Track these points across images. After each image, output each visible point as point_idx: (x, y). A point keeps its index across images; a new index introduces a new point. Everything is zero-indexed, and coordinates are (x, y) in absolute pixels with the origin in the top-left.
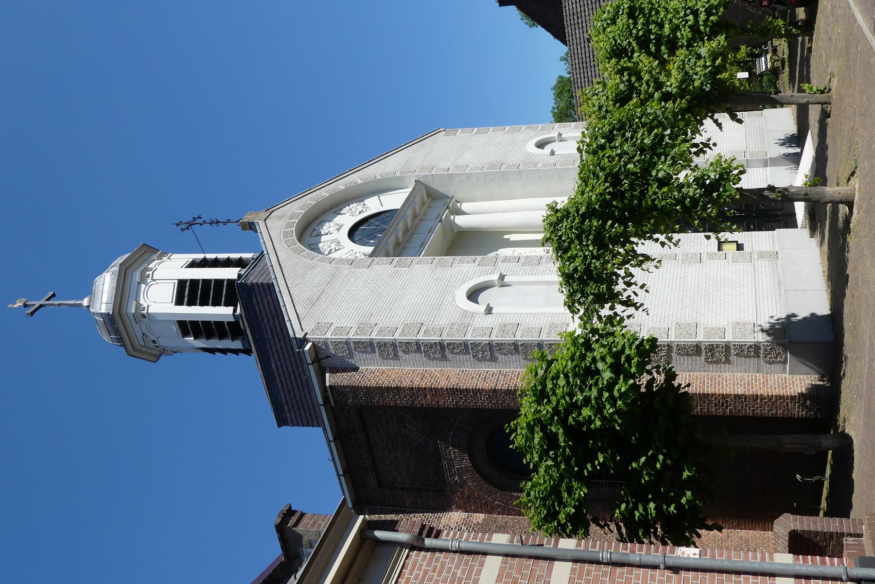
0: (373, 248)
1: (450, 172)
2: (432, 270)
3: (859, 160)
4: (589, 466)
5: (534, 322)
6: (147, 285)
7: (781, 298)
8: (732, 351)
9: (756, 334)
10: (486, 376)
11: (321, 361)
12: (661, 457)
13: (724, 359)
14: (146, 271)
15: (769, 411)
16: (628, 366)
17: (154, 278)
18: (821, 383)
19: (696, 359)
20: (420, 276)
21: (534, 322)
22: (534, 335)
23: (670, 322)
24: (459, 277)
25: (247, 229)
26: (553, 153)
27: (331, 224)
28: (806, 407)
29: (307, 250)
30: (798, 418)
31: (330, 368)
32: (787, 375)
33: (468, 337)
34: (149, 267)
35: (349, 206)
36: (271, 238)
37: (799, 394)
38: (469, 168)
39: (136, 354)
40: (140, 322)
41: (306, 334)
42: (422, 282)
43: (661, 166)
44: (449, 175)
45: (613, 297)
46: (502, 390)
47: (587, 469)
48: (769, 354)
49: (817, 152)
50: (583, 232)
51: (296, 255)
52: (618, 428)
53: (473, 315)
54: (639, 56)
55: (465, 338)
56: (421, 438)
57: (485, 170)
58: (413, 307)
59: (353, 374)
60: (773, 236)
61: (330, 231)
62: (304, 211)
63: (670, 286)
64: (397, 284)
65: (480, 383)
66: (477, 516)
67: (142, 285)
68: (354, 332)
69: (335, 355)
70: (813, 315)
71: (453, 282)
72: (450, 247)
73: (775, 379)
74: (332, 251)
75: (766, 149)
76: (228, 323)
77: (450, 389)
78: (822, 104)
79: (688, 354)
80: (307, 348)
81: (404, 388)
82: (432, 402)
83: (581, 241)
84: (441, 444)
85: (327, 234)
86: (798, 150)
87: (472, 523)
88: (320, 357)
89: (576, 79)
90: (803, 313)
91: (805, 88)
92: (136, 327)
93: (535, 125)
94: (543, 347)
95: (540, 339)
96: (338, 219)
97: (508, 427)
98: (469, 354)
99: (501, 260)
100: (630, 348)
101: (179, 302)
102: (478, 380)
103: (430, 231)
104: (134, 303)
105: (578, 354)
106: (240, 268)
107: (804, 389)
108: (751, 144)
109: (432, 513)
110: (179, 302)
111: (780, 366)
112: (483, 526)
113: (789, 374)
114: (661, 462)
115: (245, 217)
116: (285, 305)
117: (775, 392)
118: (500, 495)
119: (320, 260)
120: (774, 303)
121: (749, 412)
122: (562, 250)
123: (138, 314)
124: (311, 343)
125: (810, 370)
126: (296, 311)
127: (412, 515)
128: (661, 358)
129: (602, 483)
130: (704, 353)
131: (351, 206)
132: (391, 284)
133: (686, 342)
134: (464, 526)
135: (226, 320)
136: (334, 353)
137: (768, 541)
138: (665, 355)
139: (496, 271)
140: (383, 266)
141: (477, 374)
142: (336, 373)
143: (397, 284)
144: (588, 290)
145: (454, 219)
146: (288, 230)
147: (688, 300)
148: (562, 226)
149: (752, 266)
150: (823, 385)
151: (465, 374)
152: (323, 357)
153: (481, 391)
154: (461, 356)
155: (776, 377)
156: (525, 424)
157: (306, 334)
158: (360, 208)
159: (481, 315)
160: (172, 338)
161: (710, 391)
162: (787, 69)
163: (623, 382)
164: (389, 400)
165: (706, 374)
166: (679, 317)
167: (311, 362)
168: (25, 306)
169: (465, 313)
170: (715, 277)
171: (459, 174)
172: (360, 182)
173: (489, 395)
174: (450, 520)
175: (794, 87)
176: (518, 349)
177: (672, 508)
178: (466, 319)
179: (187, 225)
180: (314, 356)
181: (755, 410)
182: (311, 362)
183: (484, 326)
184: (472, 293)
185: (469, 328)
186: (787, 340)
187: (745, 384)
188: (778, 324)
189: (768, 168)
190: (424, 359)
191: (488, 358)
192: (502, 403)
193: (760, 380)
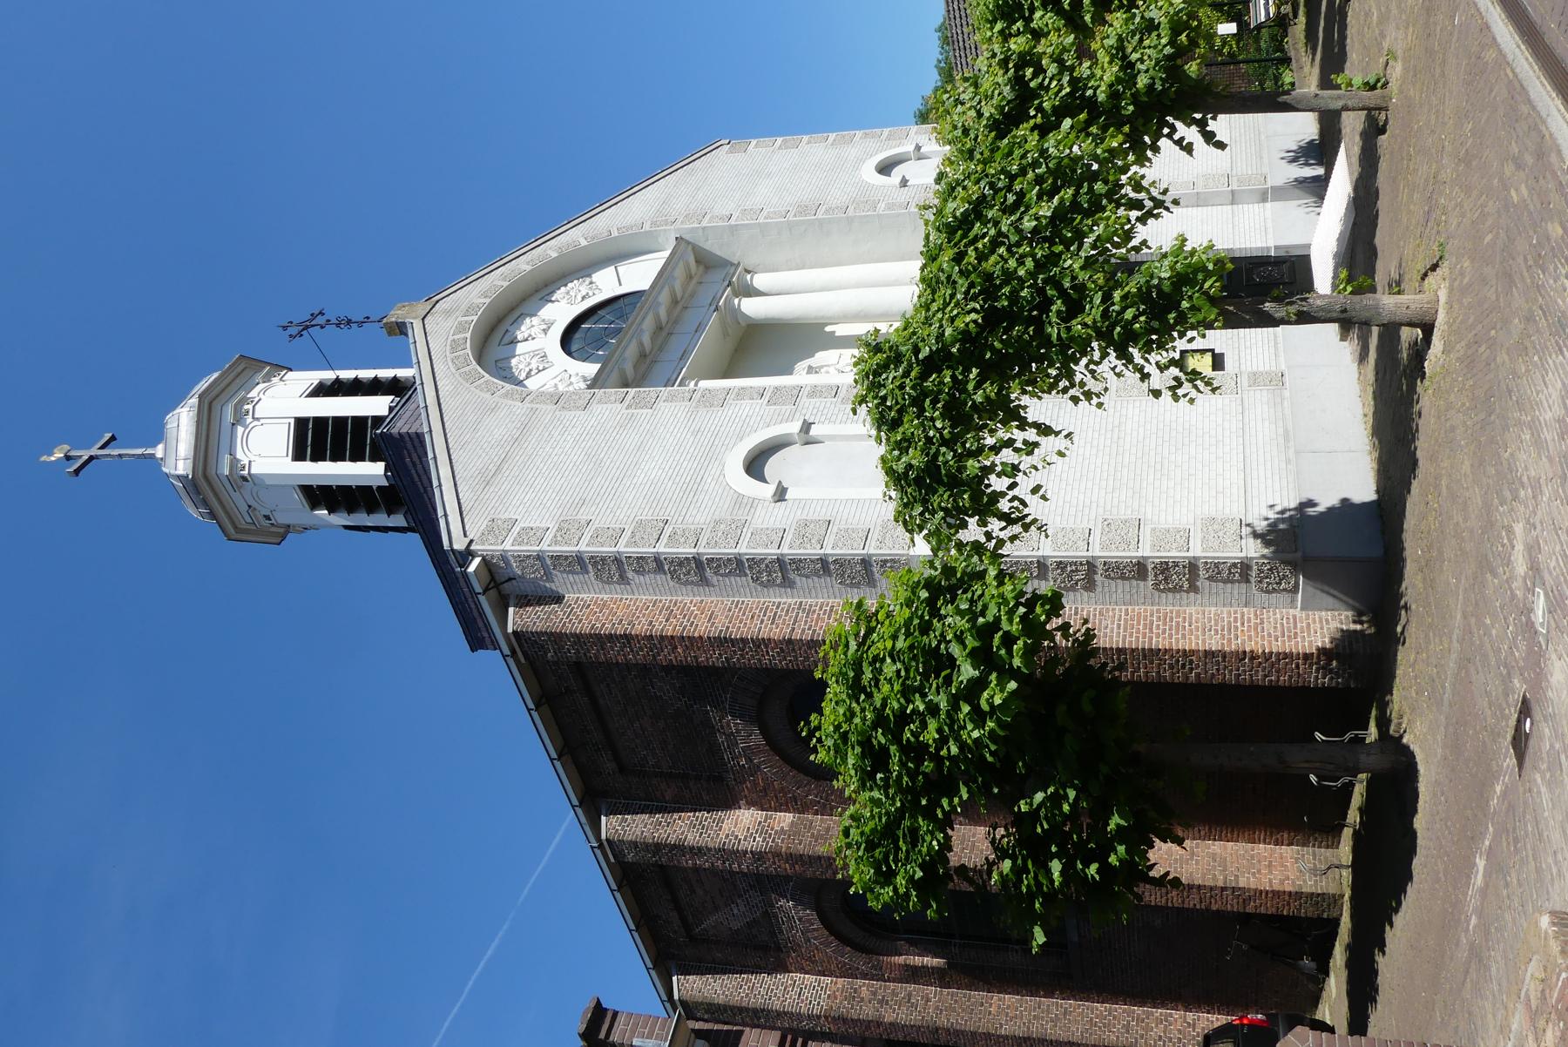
1: (732, 222)
3: (1448, 247)
4: (945, 802)
5: (857, 517)
7: (1289, 466)
8: (1202, 573)
9: (1244, 541)
10: (775, 614)
12: (1072, 794)
13: (1186, 585)
15: (1266, 676)
16: (1007, 653)
18: (1358, 627)
19: (1138, 585)
20: (668, 426)
21: (857, 517)
22: (855, 545)
23: (1093, 516)
24: (734, 425)
26: (904, 183)
27: (535, 320)
28: (1331, 671)
29: (487, 375)
30: (1316, 688)
32: (1297, 612)
33: (743, 549)
35: (566, 285)
36: (429, 353)
37: (1318, 649)
38: (765, 213)
39: (239, 536)
40: (239, 488)
41: (471, 541)
42: (672, 438)
43: (1069, 262)
45: (985, 506)
46: (801, 640)
47: (942, 807)
48: (1267, 578)
49: (1356, 189)
50: (925, 394)
51: (468, 385)
52: (990, 759)
53: (753, 502)
54: (1043, 16)
55: (736, 551)
57: (790, 217)
58: (653, 486)
59: (554, 608)
61: (533, 334)
62: (488, 301)
63: (1095, 443)
65: (766, 627)
66: (780, 817)
68: (550, 537)
69: (522, 577)
70: (1345, 502)
71: (723, 439)
72: (736, 350)
73: (1275, 619)
74: (533, 373)
75: (1265, 170)
76: (379, 488)
77: (714, 638)
78: (1369, 109)
79: (1123, 577)
80: (472, 568)
81: (637, 636)
83: (922, 410)
85: (527, 340)
86: (1320, 171)
88: (500, 579)
89: (955, 36)
90: (1327, 500)
91: (1339, 81)
92: (236, 496)
93: (878, 131)
94: (871, 566)
95: (865, 552)
96: (547, 311)
97: (804, 726)
98: (746, 575)
99: (806, 393)
100: (1010, 621)
101: (299, 455)
102: (762, 622)
103: (699, 329)
105: (916, 621)
106: (392, 397)
107: (1327, 640)
108: (1239, 160)
109: (708, 813)
110: (299, 455)
111: (1287, 596)
112: (789, 836)
113: (1302, 609)
114: (1071, 801)
115: (392, 312)
116: (440, 485)
117: (1277, 647)
118: (816, 787)
119: (506, 395)
120: (1277, 478)
121: (1230, 678)
122: (887, 422)
123: (235, 476)
124: (480, 558)
125: (1337, 604)
126: (458, 496)
127: (676, 816)
128: (1077, 584)
130: (1151, 576)
131: (570, 285)
132: (620, 442)
133: (1120, 557)
135: (375, 484)
136: (519, 573)
137: (1259, 861)
138: (1083, 579)
139: (798, 414)
140: (610, 406)
141: (762, 608)
142: (526, 606)
144: (935, 500)
145: (752, 280)
147: (1125, 471)
148: (887, 378)
149: (1239, 402)
150: (1362, 631)
152: (503, 580)
153: (767, 642)
154: (732, 579)
155: (1278, 616)
156: (831, 728)
157: (471, 541)
158: (584, 290)
159: (767, 504)
160: (295, 511)
161: (1160, 642)
162: (1302, 19)
163: (996, 685)
164: (614, 653)
165: (1155, 608)
166: (1108, 507)
167: (481, 591)
168: (68, 458)
169: (739, 500)
170: (1174, 425)
172: (584, 243)
173: (781, 649)
174: (736, 824)
175: (1314, 54)
176: (828, 568)
177: (1093, 869)
178: (740, 512)
180: (486, 578)
181: (1240, 675)
182: (481, 591)
183: (771, 525)
185: (745, 530)
186: (1299, 554)
187: (1223, 630)
188: (1283, 520)
189: (1268, 205)
190: (671, 583)
191: (778, 582)
192: (804, 661)
193: (1249, 621)
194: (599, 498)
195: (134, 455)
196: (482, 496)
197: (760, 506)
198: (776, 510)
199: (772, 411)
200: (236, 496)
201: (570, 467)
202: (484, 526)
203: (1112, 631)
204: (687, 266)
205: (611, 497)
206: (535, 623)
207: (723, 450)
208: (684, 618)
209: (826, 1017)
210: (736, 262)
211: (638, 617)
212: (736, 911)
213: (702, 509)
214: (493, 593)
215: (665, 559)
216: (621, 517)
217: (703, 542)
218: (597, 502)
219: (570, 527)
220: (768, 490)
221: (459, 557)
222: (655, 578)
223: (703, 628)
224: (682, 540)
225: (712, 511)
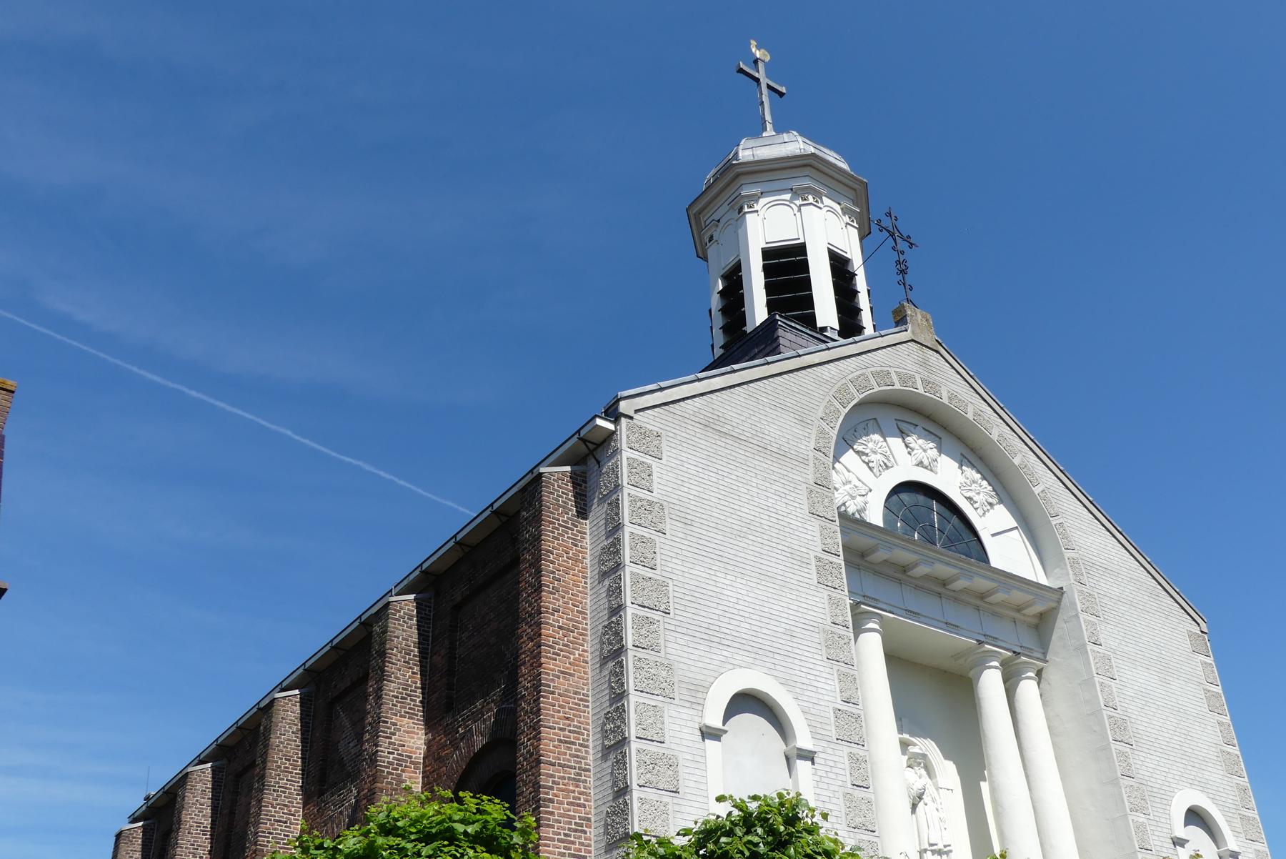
0: (882, 526)
1: (1090, 647)
2: (816, 624)
6: (791, 201)
11: (591, 457)
14: (812, 194)
17: (802, 208)
24: (803, 675)
25: (894, 318)
26: (1179, 842)
27: (934, 453)
29: (846, 410)
34: (824, 198)
38: (1109, 682)
39: (692, 217)
41: (631, 418)
44: (1084, 645)
53: (698, 704)
57: (1106, 713)
61: (915, 452)
62: (945, 401)
64: (773, 564)
67: (790, 195)
69: (600, 474)
72: (945, 672)
74: (864, 457)
77: (540, 680)
82: (523, 653)
84: (500, 691)
85: (907, 446)
87: (403, 771)
92: (725, 207)
93: (1253, 804)
99: (854, 751)
101: (767, 254)
103: (948, 625)
104: (757, 190)
106: (838, 329)
109: (421, 702)
110: (767, 254)
119: (822, 431)
124: (614, 429)
127: (417, 669)
131: (985, 483)
134: (394, 758)
136: (604, 470)
140: (818, 539)
141: (580, 727)
143: (773, 564)
153: (537, 738)
157: (631, 418)
160: (720, 261)
168: (756, 61)
171: (1090, 664)
174: (408, 732)
178: (684, 692)
179: (891, 229)
184: (763, 702)
185: (660, 698)
190: (600, 627)
191: (606, 743)
192: (522, 780)
194: (695, 539)
195: (764, 114)
196: (690, 422)
197: (695, 712)
198: (690, 731)
199: (827, 715)
200: (725, 207)
201: (732, 506)
202: (651, 428)
204: (1029, 604)
205: (697, 551)
206: (552, 493)
207: (768, 665)
208: (564, 645)
209: (255, 851)
210: (1048, 658)
211: (563, 597)
212: (352, 745)
213: (686, 649)
214: (583, 448)
215: (620, 616)
216: (670, 565)
217: (641, 654)
218: (689, 538)
219: (655, 513)
220: (715, 720)
221: (613, 408)
222: (605, 609)
223: (551, 666)
224: (643, 631)
225: (682, 660)
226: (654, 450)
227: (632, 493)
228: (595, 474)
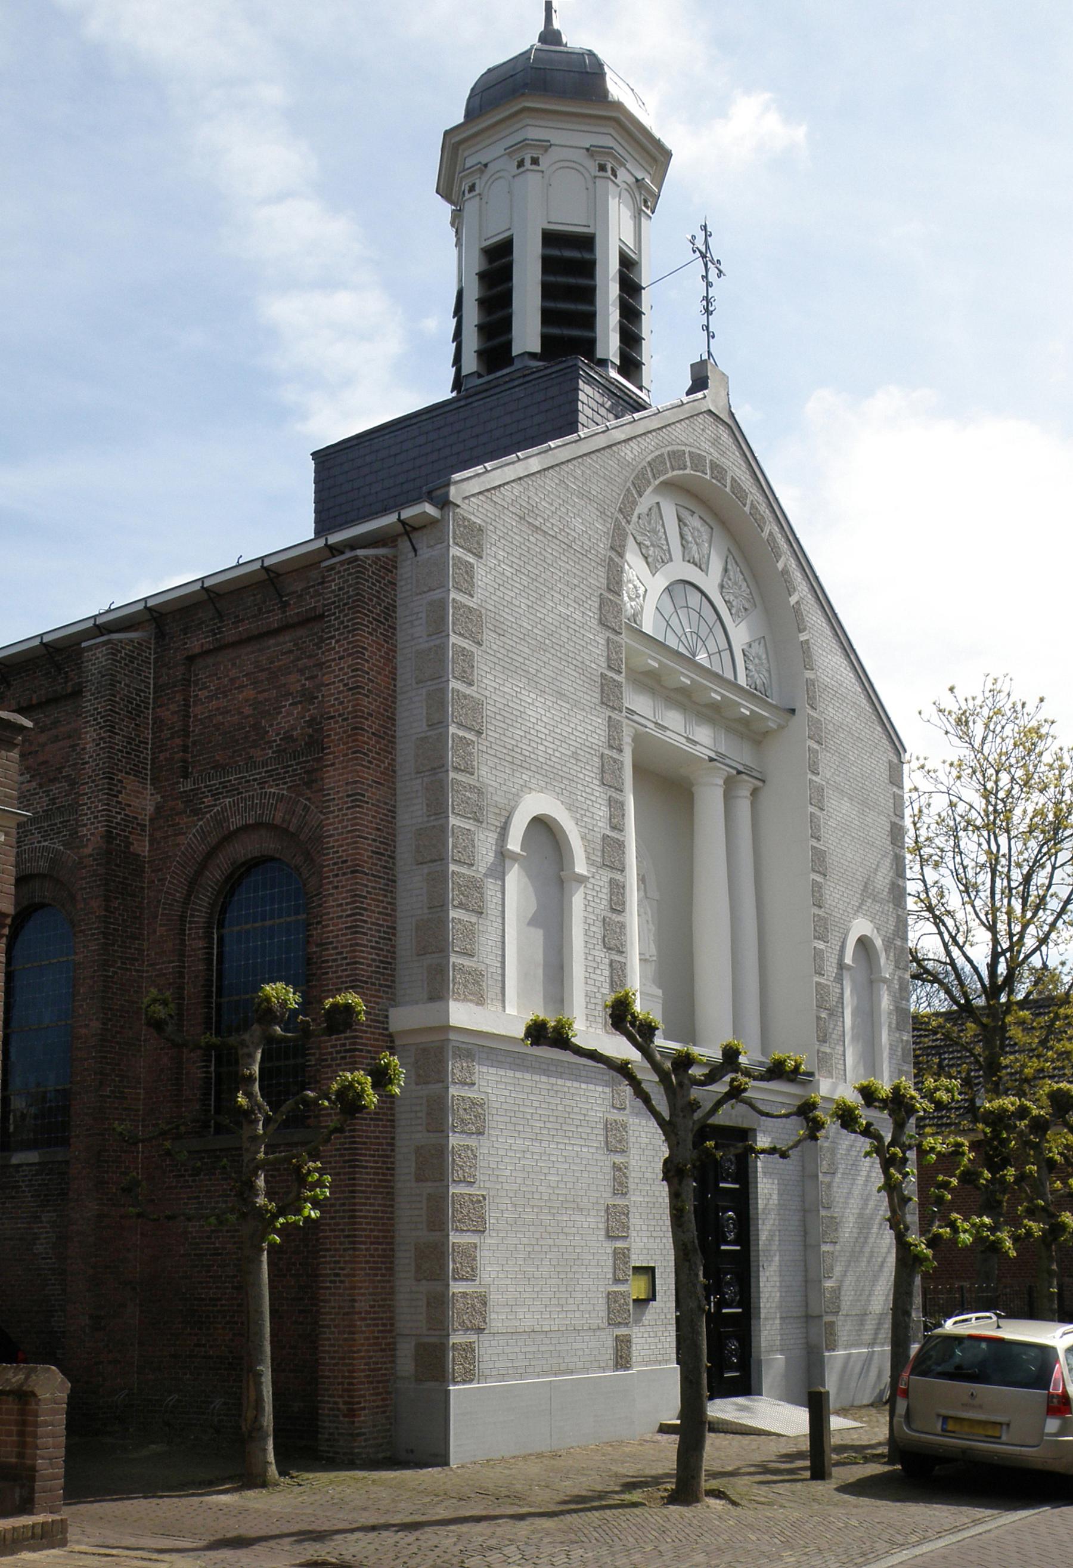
10: (383, 855)
11: (406, 538)
31: (395, 557)
38: (818, 813)
56: (278, 734)
60: (667, 1362)
68: (463, 600)
88: (415, 536)
92: (499, 149)
101: (550, 238)
102: (374, 840)
106: (618, 363)
110: (550, 238)
129: (210, 1067)
146: (688, 459)
151: (387, 816)
187: (375, 1313)
203: (371, 1205)
208: (377, 753)
217: (460, 777)
226: (474, 537)
227: (458, 598)
228: (409, 562)
